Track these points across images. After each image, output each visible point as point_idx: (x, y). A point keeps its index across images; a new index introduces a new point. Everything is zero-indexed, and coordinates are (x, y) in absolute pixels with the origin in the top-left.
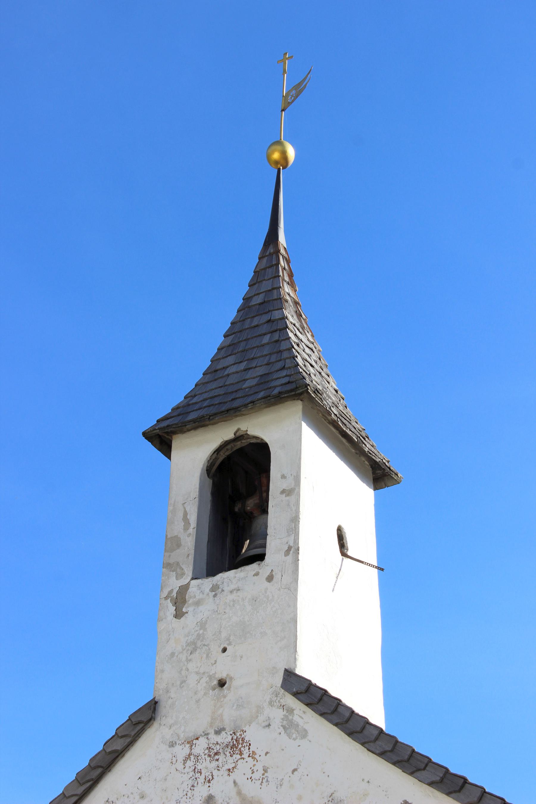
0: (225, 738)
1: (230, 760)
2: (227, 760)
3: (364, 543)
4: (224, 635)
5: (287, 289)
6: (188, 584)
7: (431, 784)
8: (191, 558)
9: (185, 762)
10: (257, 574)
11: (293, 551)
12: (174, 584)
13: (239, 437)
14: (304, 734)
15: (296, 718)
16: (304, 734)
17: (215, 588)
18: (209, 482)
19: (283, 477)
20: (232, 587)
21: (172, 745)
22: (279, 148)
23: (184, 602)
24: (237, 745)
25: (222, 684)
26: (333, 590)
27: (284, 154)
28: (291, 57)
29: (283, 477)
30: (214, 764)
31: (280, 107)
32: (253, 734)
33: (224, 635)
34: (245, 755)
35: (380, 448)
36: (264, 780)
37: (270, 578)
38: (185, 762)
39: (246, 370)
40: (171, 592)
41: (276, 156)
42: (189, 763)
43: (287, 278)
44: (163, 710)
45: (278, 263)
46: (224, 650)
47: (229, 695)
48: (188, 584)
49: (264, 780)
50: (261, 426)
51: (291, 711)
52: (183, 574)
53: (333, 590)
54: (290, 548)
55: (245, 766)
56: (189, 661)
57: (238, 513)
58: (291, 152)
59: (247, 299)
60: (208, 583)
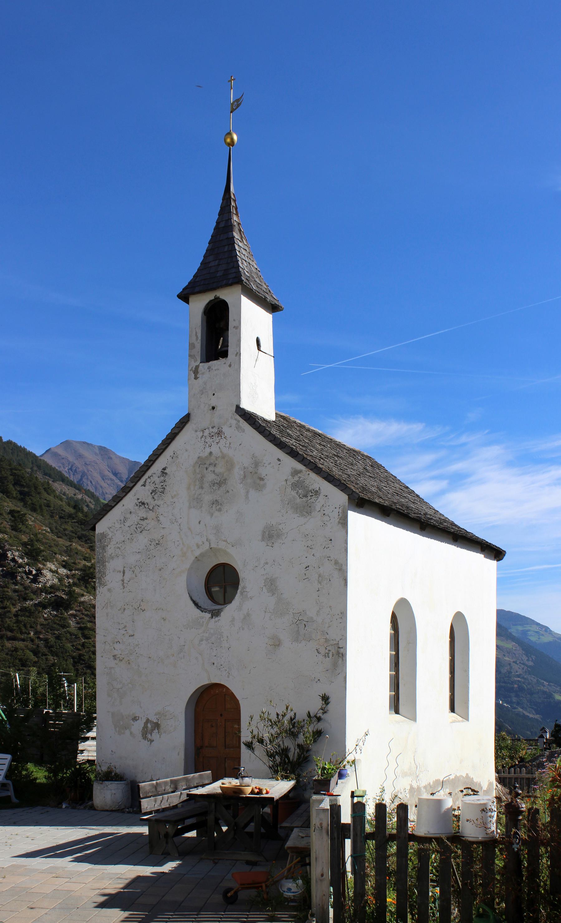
0: (215, 430)
1: (218, 439)
2: (216, 439)
3: (268, 344)
4: (213, 388)
5: (235, 218)
6: (199, 365)
7: (287, 453)
8: (200, 353)
9: (201, 438)
10: (225, 363)
11: (238, 354)
12: (194, 364)
13: (217, 298)
14: (243, 431)
15: (241, 424)
16: (243, 431)
17: (209, 368)
18: (205, 317)
19: (234, 320)
20: (216, 368)
21: (196, 431)
22: (229, 136)
23: (198, 373)
24: (220, 433)
25: (213, 408)
26: (258, 341)
27: (232, 139)
28: (234, 79)
29: (234, 320)
30: (212, 440)
31: (230, 110)
32: (225, 429)
33: (213, 388)
34: (223, 437)
35: (275, 297)
36: (230, 447)
37: (230, 366)
38: (201, 438)
39: (219, 265)
40: (192, 368)
41: (228, 140)
42: (203, 439)
43: (234, 212)
44: (192, 417)
45: (231, 204)
46: (214, 394)
47: (217, 412)
48: (199, 365)
49: (230, 447)
50: (225, 294)
51: (239, 421)
52: (197, 360)
53: (258, 341)
54: (237, 353)
55: (223, 442)
56: (201, 398)
57: (217, 338)
58: (235, 137)
59: (218, 223)
60: (207, 365)
